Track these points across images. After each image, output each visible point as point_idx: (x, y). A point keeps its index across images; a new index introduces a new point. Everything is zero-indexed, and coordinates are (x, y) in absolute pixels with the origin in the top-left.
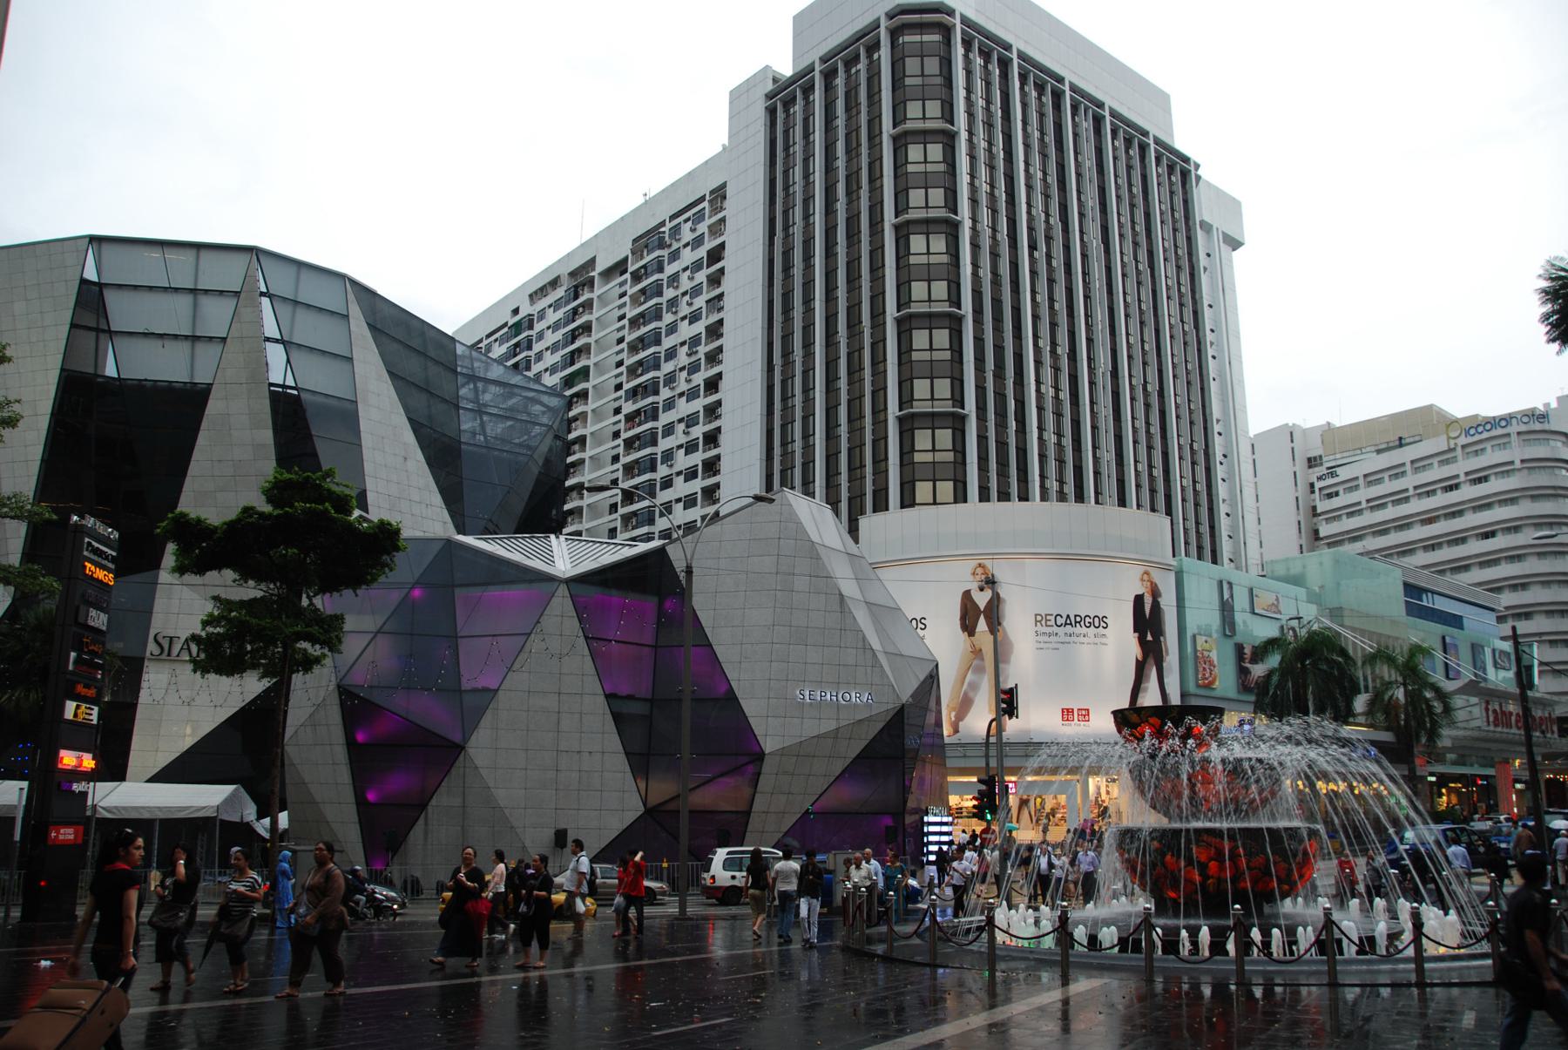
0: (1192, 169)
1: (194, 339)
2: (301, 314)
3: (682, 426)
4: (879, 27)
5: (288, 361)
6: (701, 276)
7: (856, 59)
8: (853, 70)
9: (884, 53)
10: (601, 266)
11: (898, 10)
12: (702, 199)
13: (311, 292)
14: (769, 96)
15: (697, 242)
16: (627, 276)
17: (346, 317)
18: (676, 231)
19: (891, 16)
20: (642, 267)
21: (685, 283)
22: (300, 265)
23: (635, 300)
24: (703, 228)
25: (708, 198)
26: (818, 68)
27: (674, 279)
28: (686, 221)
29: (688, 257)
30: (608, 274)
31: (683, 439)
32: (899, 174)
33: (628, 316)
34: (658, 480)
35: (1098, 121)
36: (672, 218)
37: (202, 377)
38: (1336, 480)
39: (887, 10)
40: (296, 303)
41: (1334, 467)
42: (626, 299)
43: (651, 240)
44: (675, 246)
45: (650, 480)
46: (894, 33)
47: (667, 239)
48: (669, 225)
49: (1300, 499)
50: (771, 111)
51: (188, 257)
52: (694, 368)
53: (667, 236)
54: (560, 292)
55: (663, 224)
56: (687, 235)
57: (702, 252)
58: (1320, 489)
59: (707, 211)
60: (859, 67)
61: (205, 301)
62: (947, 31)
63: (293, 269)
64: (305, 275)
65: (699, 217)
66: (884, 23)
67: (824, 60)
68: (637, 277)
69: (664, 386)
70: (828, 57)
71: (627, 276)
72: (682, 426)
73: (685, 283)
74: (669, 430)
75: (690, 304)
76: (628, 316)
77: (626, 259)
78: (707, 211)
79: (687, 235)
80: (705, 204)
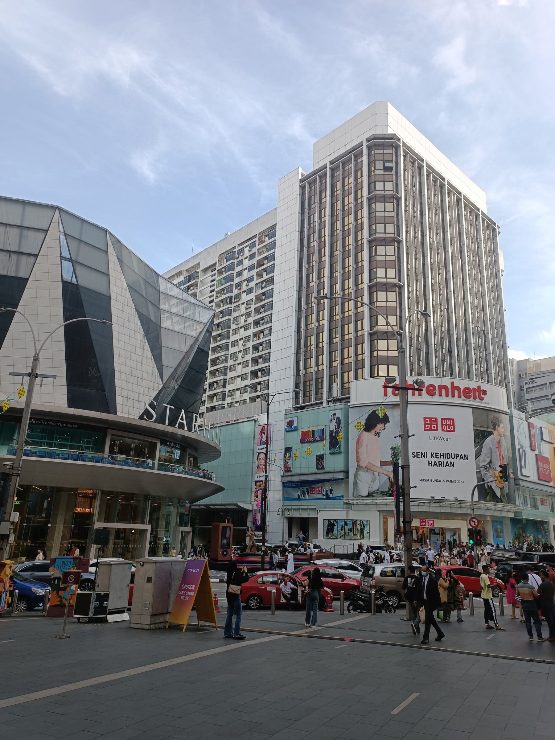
0: (497, 228)
1: (19, 253)
2: (83, 247)
3: (241, 342)
4: (362, 145)
5: (74, 271)
6: (254, 272)
7: (349, 160)
8: (347, 168)
9: (365, 158)
10: (202, 267)
11: (373, 137)
12: (255, 236)
13: (89, 236)
14: (301, 181)
15: (252, 257)
16: (216, 272)
17: (107, 252)
18: (241, 251)
19: (368, 140)
20: (223, 268)
21: (246, 274)
22: (83, 221)
23: (219, 284)
24: (255, 250)
25: (258, 236)
26: (328, 167)
27: (240, 274)
28: (246, 247)
29: (247, 263)
30: (205, 270)
31: (242, 348)
32: (371, 217)
33: (216, 290)
34: (229, 367)
35: (459, 200)
36: (239, 245)
37: (22, 274)
38: (535, 385)
39: (367, 137)
40: (80, 241)
41: (534, 379)
42: (215, 282)
43: (229, 255)
44: (240, 258)
45: (225, 367)
46: (369, 148)
47: (236, 255)
48: (237, 249)
49: (516, 393)
50: (303, 188)
51: (18, 208)
52: (249, 315)
53: (236, 253)
54: (181, 278)
55: (234, 248)
56: (247, 253)
57: (254, 261)
58: (527, 389)
59: (257, 242)
60: (338, 173)
61: (26, 232)
62: (397, 148)
63: (78, 223)
64: (85, 226)
65: (253, 245)
66: (365, 144)
67: (331, 163)
68: (220, 272)
69: (233, 323)
70: (338, 159)
71: (216, 272)
72: (241, 342)
73: (246, 274)
74: (235, 343)
75: (247, 286)
76: (216, 290)
77: (215, 264)
78: (257, 242)
79: (247, 253)
80: (257, 239)
